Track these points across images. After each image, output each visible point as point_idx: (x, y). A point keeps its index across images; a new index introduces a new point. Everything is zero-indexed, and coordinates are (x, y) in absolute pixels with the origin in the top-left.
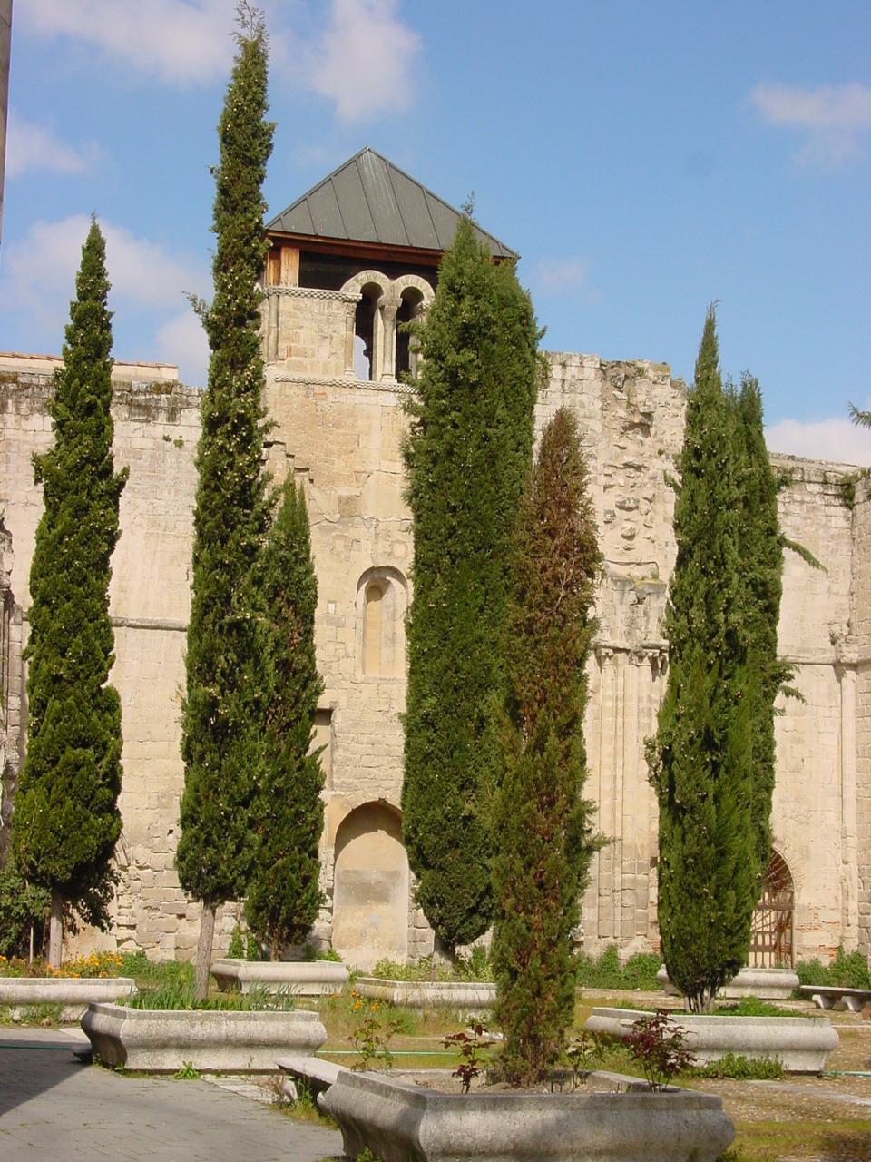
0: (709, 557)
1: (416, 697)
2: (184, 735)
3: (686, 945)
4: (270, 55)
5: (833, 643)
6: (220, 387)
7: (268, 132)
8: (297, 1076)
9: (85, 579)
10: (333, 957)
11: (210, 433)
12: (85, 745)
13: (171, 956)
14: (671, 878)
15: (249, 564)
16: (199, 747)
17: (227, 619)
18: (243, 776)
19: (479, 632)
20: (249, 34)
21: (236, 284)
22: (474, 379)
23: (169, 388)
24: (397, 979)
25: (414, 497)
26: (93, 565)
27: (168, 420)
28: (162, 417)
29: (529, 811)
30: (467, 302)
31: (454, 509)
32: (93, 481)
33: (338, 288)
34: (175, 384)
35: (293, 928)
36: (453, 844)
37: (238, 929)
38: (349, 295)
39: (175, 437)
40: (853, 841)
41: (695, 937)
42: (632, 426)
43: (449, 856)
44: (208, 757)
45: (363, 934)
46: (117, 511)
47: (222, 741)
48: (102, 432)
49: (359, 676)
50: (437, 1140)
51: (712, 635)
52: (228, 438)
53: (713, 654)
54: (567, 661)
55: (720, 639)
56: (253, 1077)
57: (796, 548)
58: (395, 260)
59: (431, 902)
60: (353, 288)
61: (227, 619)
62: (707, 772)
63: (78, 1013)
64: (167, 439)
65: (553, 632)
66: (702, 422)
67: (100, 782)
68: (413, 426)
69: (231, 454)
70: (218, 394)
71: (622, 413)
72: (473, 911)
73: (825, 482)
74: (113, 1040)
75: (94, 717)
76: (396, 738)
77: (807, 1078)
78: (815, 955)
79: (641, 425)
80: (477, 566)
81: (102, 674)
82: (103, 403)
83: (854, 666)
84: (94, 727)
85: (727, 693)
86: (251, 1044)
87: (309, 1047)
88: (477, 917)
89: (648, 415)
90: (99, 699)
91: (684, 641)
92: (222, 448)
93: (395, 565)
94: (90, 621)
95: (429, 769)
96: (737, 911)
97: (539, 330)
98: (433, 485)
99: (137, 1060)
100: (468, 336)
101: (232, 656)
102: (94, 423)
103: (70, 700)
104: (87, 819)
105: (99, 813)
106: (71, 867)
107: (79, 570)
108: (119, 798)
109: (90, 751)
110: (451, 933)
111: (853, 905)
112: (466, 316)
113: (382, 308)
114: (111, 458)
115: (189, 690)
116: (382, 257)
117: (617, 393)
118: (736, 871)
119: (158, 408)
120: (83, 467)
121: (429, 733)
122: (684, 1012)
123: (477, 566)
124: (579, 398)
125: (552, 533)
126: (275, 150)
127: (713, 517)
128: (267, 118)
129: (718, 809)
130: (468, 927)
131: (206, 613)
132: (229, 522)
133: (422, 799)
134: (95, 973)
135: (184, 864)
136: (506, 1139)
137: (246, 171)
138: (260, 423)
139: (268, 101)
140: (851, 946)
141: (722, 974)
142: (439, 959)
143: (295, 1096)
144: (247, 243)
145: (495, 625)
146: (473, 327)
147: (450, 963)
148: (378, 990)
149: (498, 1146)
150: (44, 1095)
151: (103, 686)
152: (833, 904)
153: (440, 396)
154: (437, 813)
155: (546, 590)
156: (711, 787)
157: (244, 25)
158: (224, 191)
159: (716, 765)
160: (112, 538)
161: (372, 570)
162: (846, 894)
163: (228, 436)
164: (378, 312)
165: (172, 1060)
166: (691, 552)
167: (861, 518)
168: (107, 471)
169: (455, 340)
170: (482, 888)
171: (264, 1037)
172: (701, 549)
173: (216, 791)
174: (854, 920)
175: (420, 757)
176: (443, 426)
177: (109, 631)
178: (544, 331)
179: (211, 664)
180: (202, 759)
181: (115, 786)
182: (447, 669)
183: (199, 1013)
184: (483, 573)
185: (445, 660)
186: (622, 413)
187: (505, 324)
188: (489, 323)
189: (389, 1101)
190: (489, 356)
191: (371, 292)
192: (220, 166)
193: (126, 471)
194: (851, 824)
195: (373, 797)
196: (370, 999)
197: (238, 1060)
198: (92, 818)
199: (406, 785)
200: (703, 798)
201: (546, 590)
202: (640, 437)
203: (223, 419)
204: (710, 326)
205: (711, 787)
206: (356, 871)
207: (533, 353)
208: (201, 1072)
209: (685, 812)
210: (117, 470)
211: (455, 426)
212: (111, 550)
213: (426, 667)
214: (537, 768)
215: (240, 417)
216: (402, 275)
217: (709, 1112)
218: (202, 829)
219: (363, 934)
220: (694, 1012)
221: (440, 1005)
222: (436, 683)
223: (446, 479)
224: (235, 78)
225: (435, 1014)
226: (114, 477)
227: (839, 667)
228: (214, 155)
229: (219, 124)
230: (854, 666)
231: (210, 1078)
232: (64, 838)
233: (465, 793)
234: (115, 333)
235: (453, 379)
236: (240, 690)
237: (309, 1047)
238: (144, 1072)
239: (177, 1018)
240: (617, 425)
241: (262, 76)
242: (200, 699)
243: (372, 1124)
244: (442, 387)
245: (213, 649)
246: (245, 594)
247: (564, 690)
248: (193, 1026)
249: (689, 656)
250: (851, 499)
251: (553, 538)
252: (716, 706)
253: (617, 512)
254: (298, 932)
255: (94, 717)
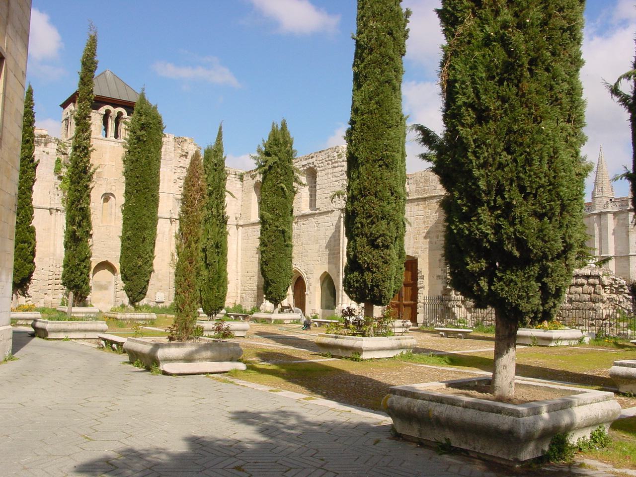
0: (218, 194)
1: (125, 230)
2: (65, 241)
3: (208, 302)
4: (98, 40)
5: (236, 219)
6: (79, 137)
7: (96, 63)
8: (104, 340)
9: (25, 193)
10: (92, 306)
11: (75, 151)
12: (25, 243)
13: (42, 305)
14: (205, 284)
15: (86, 191)
16: (70, 244)
17: (79, 206)
18: (83, 253)
19: (144, 213)
20: (92, 34)
21: (85, 107)
22: (145, 139)
23: (45, 136)
24: (118, 312)
25: (126, 173)
26: (28, 189)
27: (45, 146)
28: (43, 145)
29: (185, 264)
30: (144, 117)
31: (138, 177)
32: (28, 163)
33: (98, 110)
34: (47, 135)
35: (82, 297)
36: (135, 274)
37: (63, 298)
38: (101, 112)
39: (47, 151)
40: (240, 274)
41: (211, 300)
42: (183, 156)
43: (134, 277)
44: (73, 247)
45: (101, 299)
46: (35, 172)
47: (77, 243)
48: (31, 149)
49: (101, 225)
50: (163, 356)
51: (218, 216)
52: (81, 153)
53: (218, 221)
54: (197, 222)
55: (220, 217)
56: (86, 340)
57: (229, 192)
58: (115, 103)
59: (128, 290)
60: (103, 110)
61: (79, 206)
62: (216, 255)
63: (30, 323)
64: (44, 152)
65: (193, 214)
66: (217, 155)
67: (29, 254)
68: (126, 152)
69: (82, 158)
70: (78, 139)
71: (180, 152)
72: (140, 293)
73: (236, 174)
74: (44, 330)
75: (28, 234)
76: (119, 243)
77: (241, 338)
78: (228, 305)
79: (185, 155)
80: (144, 194)
81: (30, 222)
82: (32, 140)
83: (242, 226)
84: (28, 238)
85: (222, 232)
86: (86, 331)
87: (103, 331)
88: (141, 294)
89: (187, 153)
90: (29, 229)
91: (210, 218)
92: (79, 156)
93: (112, 192)
94: (27, 205)
95: (128, 252)
96: (223, 293)
97: (164, 127)
98: (132, 169)
99: (51, 336)
100: (143, 127)
101: (80, 218)
102: (29, 146)
103: (20, 229)
104: (25, 265)
105: (29, 263)
106: (20, 279)
107: (23, 190)
108: (35, 259)
109: (26, 244)
110: (134, 299)
111: (239, 292)
112: (143, 121)
113: (111, 117)
114: (34, 156)
115: (67, 227)
116: (111, 102)
117: (178, 146)
118: (223, 282)
119: (41, 142)
120: (25, 159)
121: (129, 242)
122: (207, 320)
123: (144, 194)
124: (168, 147)
125: (193, 186)
126: (98, 68)
127: (219, 183)
128: (96, 59)
129: (219, 264)
130: (139, 297)
131: (72, 204)
132: (80, 178)
133: (126, 261)
134: (27, 311)
135: (64, 279)
136: (181, 356)
137: (89, 73)
138: (90, 149)
139: (97, 54)
140: (238, 303)
141: (218, 310)
142: (130, 306)
143: (104, 345)
144: (88, 95)
145: (149, 211)
146: (145, 124)
147: (133, 308)
148: (112, 315)
149: (179, 358)
150: (26, 346)
151: (30, 225)
152: (233, 291)
153: (134, 144)
154: (130, 265)
155: (192, 202)
156: (217, 259)
157: (91, 30)
158: (82, 79)
159: (218, 252)
160: (34, 181)
161: (106, 193)
162: (237, 288)
163: (81, 152)
164: (110, 118)
165: (62, 335)
166: (213, 192)
167: (245, 185)
168: (32, 161)
169: (139, 128)
170: (143, 286)
171: (89, 329)
172: (216, 191)
173: (75, 257)
174: (239, 295)
175: (126, 249)
176: (135, 152)
177: (32, 209)
178: (165, 127)
179: (74, 219)
180: (70, 248)
181: (34, 255)
182: (135, 223)
183: (70, 322)
184: (146, 196)
185: (134, 221)
186: (180, 152)
187: (154, 124)
188: (150, 123)
189: (146, 346)
190: (149, 133)
191: (108, 112)
192: (81, 71)
193: (39, 161)
194: (239, 269)
195: (104, 260)
196: (110, 318)
197: (82, 335)
198: (27, 265)
199: (121, 256)
200: (215, 262)
201: (192, 202)
202: (185, 159)
203: (79, 147)
204: (220, 128)
205: (217, 259)
206: (99, 281)
207: (162, 133)
208: (71, 339)
209: (209, 265)
210: (36, 160)
211: (139, 153)
212: (34, 184)
213: (128, 223)
214: (188, 252)
215: (85, 146)
216: (101, 107)
217: (236, 347)
218: (70, 268)
219: (101, 299)
220: (210, 320)
221: (131, 320)
222: (131, 227)
223: (136, 168)
224: (87, 46)
225: (129, 322)
226: (35, 162)
227: (238, 226)
228: (79, 68)
229: (81, 59)
230: (242, 226)
231: (73, 340)
232: (18, 270)
233: (139, 259)
234: (36, 118)
235: (138, 139)
236: (82, 228)
237: (103, 331)
238: (53, 339)
239: (64, 323)
240: (179, 155)
241: (95, 46)
242: (71, 230)
243: (140, 353)
244: (135, 141)
245: (75, 215)
246: (85, 199)
247: (196, 230)
248: (68, 326)
249: (211, 222)
250: (242, 179)
251: (194, 187)
252: (219, 237)
253: (178, 180)
254: (84, 299)
255: (28, 234)
